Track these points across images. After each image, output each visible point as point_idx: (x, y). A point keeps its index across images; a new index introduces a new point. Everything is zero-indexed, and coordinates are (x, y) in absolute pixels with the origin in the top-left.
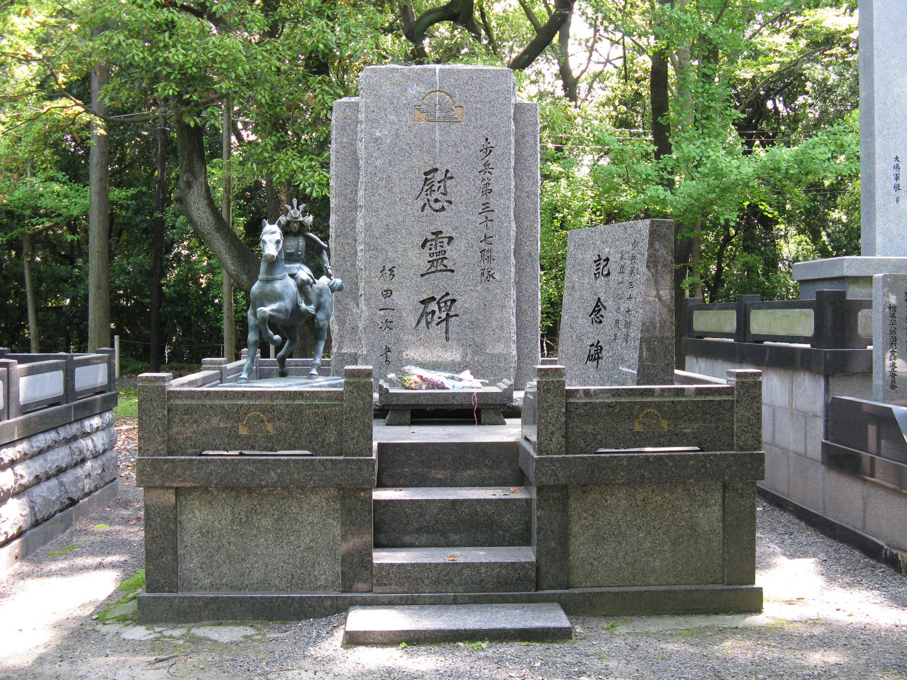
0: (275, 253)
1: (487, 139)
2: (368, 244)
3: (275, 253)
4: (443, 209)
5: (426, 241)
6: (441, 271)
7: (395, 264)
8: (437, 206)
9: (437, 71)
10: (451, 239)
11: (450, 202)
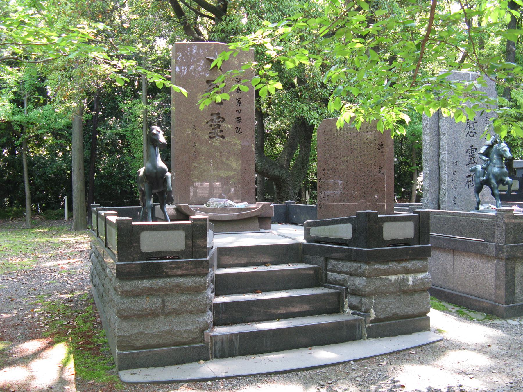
0: (61, 351)
1: (380, 168)
2: (448, 151)
3: (61, 351)
4: (473, 136)
5: (468, 150)
6: (472, 163)
7: (458, 160)
8: (471, 134)
9: (121, 352)
10: (476, 149)
11: (476, 133)
